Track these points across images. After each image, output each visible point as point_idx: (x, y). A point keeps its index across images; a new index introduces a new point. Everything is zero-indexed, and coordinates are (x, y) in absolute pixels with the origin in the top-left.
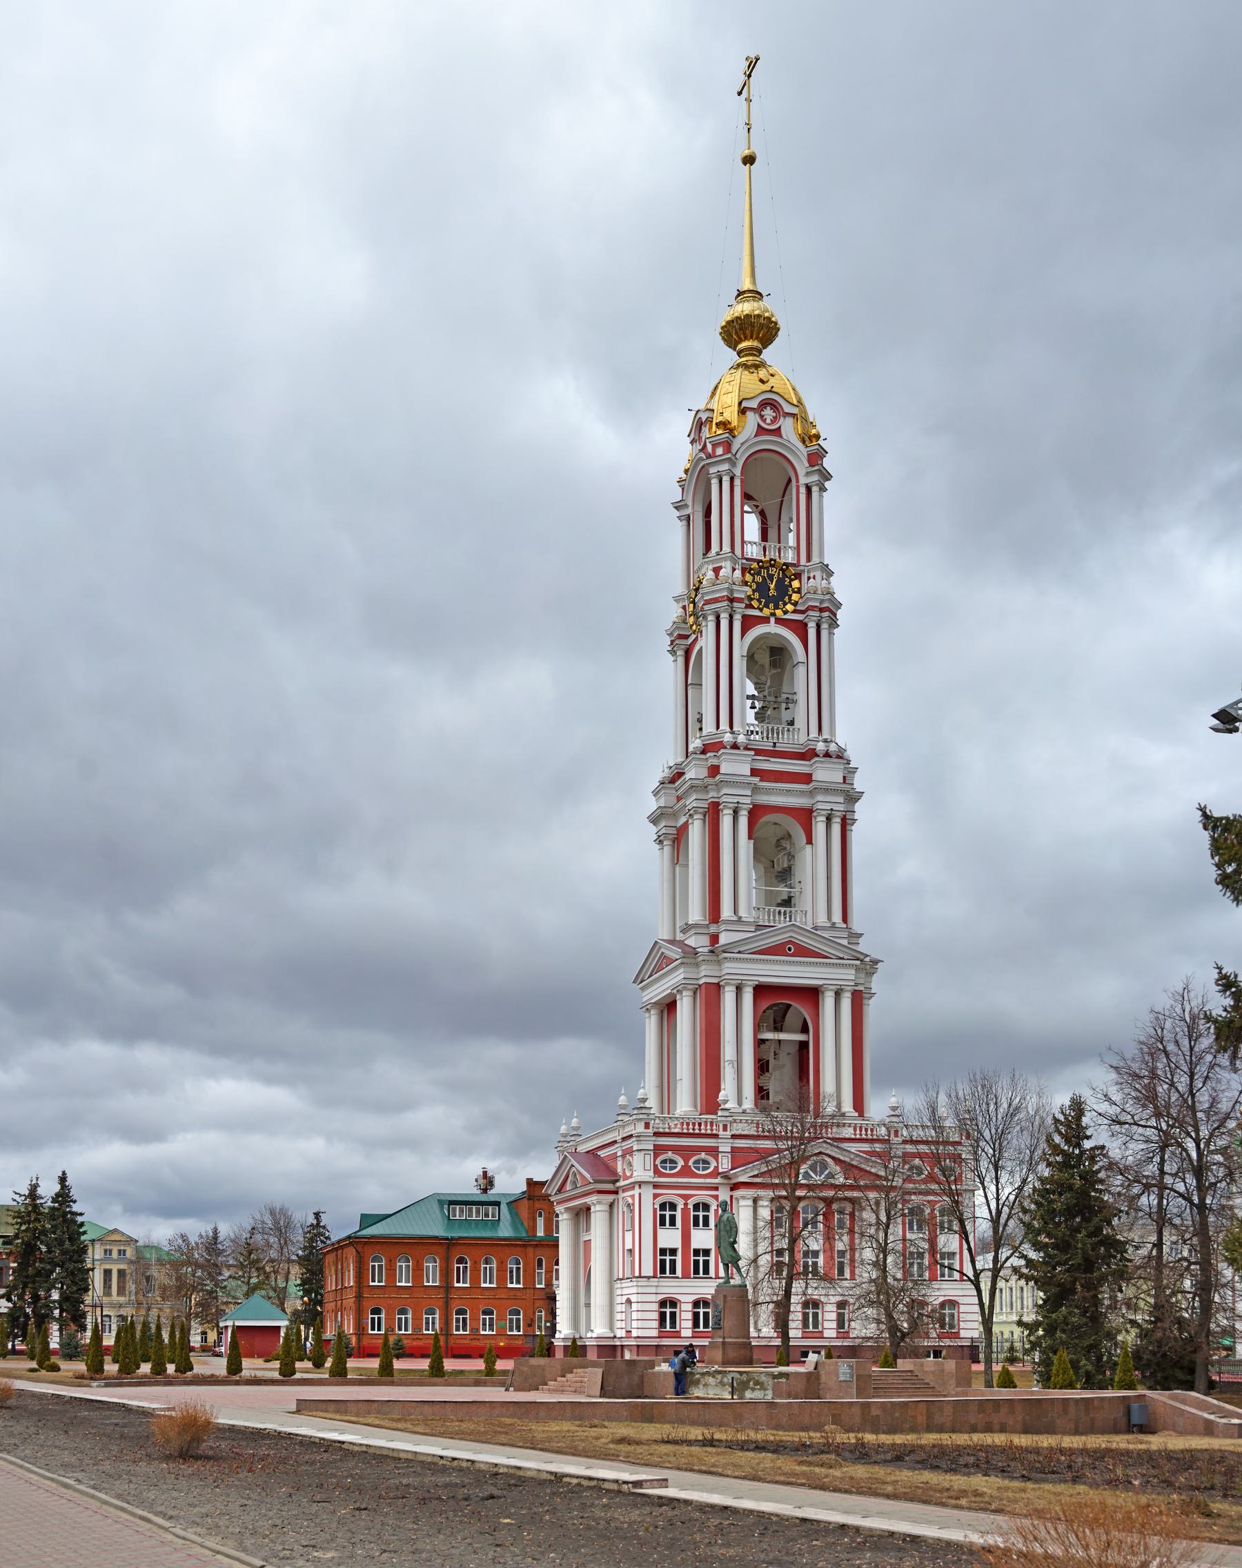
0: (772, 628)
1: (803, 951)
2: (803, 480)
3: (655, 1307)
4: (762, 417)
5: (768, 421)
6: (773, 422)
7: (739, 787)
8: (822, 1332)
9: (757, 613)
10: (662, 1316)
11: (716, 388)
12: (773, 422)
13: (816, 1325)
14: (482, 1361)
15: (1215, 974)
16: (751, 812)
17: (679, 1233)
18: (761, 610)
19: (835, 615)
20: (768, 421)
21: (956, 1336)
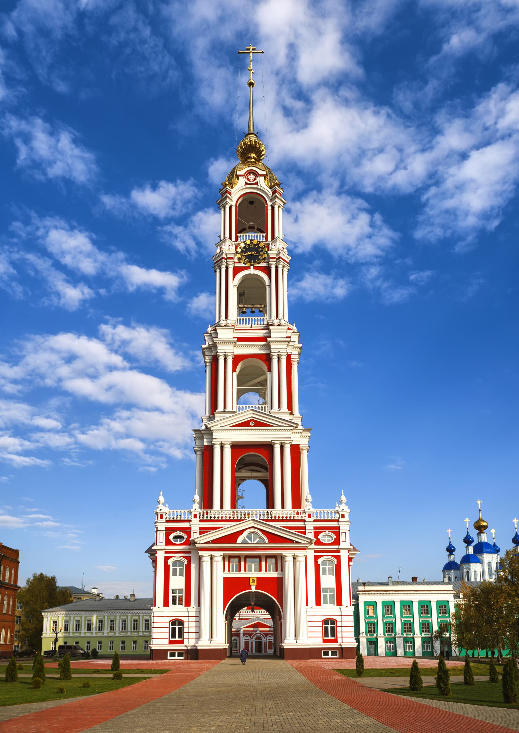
0: (252, 271)
1: (259, 424)
3: (321, 624)
4: (248, 179)
5: (251, 180)
6: (253, 181)
7: (144, 668)
9: (243, 265)
12: (253, 181)
16: (234, 359)
18: (245, 264)
20: (251, 180)
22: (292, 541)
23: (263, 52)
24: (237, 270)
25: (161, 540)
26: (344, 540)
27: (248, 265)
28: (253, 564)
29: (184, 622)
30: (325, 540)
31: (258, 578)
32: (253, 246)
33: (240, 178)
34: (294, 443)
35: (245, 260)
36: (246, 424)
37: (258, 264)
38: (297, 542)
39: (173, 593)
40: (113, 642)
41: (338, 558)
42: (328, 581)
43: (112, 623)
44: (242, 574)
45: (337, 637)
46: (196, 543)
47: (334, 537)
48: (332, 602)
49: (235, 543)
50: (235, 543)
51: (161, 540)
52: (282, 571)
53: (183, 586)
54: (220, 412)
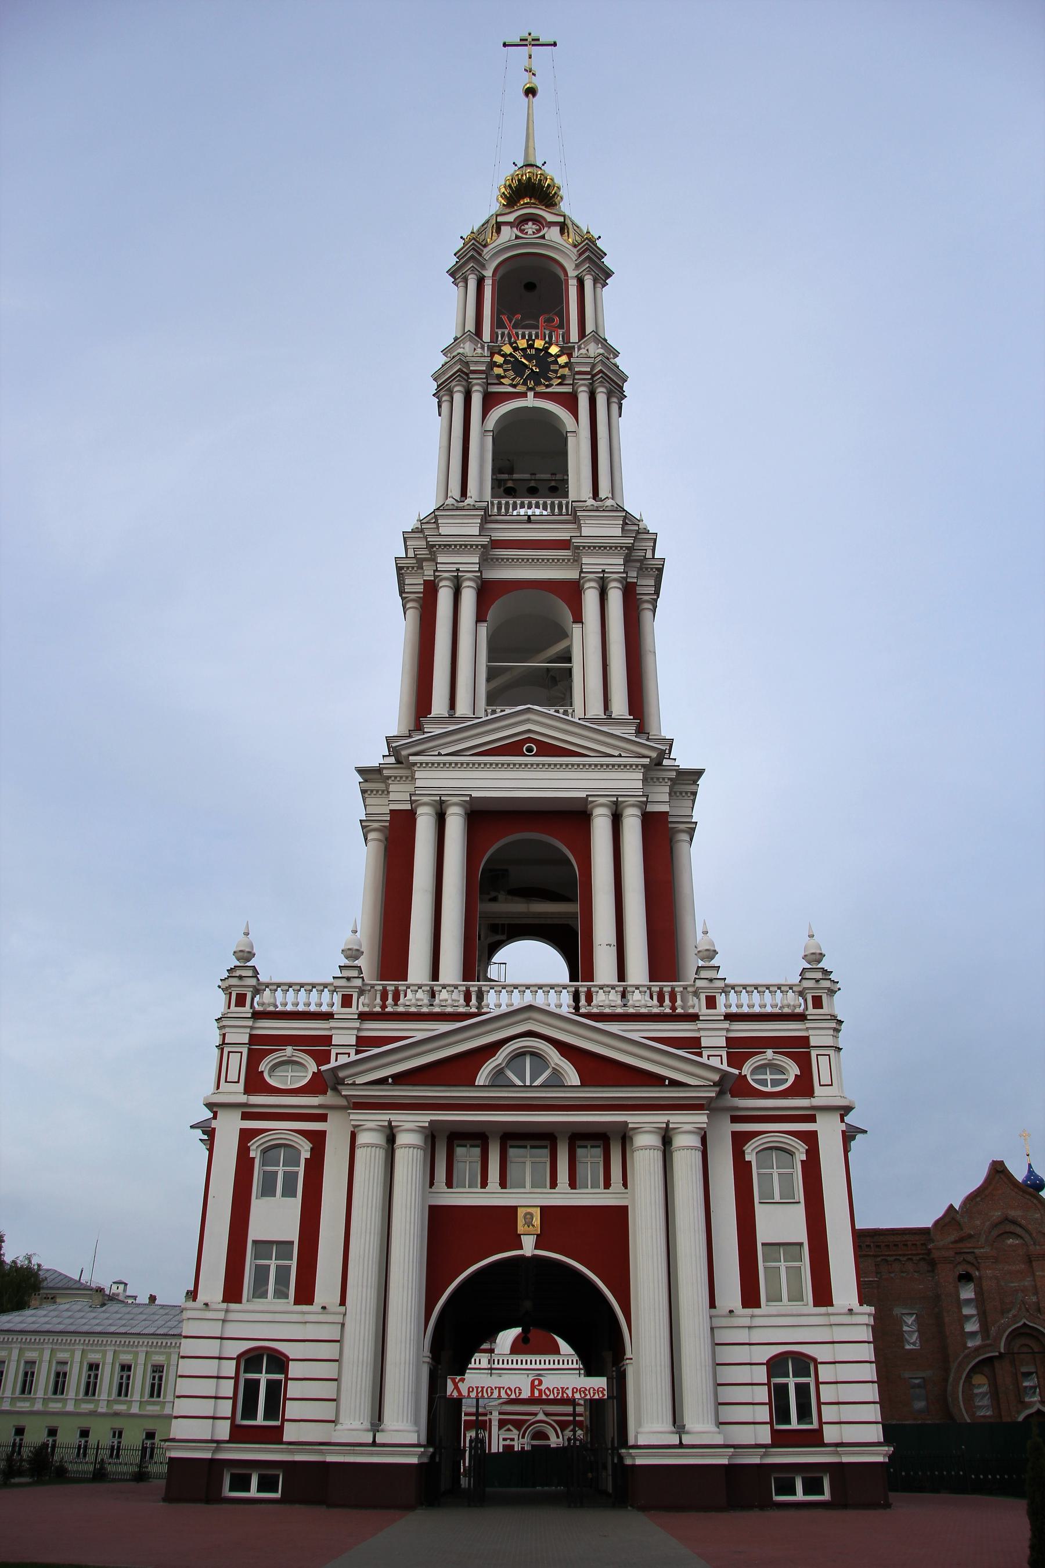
0: (531, 401)
2: (572, 273)
3: (761, 1374)
8: (820, 1432)
10: (779, 1394)
11: (536, 42)
13: (804, 1413)
14: (604, 1379)
15: (237, 942)
17: (801, 1209)
18: (514, 386)
19: (622, 388)
21: (814, 1438)
22: (657, 1080)
23: (555, 44)
24: (490, 401)
25: (233, 1076)
26: (825, 1080)
27: (521, 389)
28: (527, 1162)
29: (288, 1359)
30: (764, 1082)
31: (546, 1211)
32: (533, 352)
33: (503, 228)
34: (651, 808)
35: (513, 380)
36: (513, 748)
37: (547, 386)
38: (674, 1083)
39: (257, 1257)
40: (120, 1433)
41: (811, 1139)
42: (781, 1222)
43: (125, 1374)
44: (493, 1197)
45: (821, 1423)
46: (341, 1082)
47: (793, 1070)
48: (796, 1296)
49: (471, 1083)
50: (471, 1083)
51: (233, 1076)
52: (625, 1185)
53: (292, 1233)
54: (439, 720)
